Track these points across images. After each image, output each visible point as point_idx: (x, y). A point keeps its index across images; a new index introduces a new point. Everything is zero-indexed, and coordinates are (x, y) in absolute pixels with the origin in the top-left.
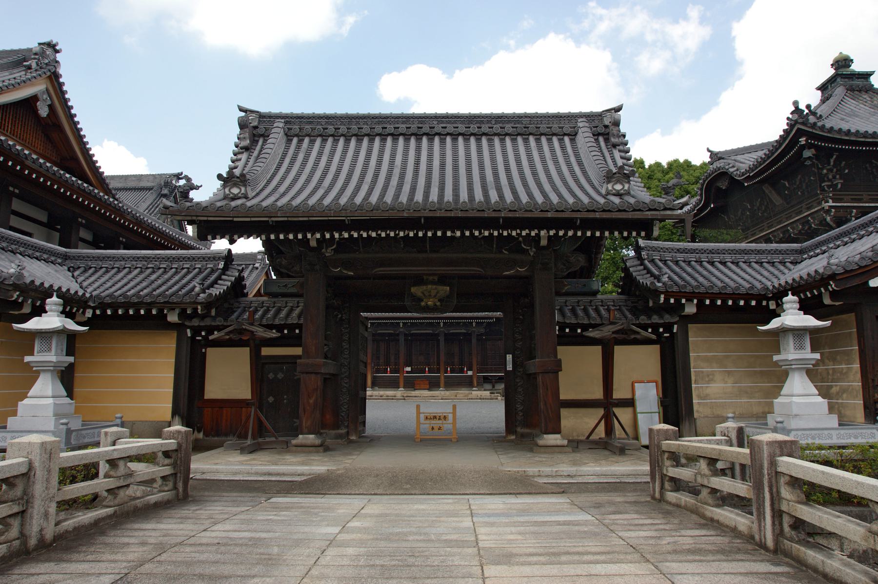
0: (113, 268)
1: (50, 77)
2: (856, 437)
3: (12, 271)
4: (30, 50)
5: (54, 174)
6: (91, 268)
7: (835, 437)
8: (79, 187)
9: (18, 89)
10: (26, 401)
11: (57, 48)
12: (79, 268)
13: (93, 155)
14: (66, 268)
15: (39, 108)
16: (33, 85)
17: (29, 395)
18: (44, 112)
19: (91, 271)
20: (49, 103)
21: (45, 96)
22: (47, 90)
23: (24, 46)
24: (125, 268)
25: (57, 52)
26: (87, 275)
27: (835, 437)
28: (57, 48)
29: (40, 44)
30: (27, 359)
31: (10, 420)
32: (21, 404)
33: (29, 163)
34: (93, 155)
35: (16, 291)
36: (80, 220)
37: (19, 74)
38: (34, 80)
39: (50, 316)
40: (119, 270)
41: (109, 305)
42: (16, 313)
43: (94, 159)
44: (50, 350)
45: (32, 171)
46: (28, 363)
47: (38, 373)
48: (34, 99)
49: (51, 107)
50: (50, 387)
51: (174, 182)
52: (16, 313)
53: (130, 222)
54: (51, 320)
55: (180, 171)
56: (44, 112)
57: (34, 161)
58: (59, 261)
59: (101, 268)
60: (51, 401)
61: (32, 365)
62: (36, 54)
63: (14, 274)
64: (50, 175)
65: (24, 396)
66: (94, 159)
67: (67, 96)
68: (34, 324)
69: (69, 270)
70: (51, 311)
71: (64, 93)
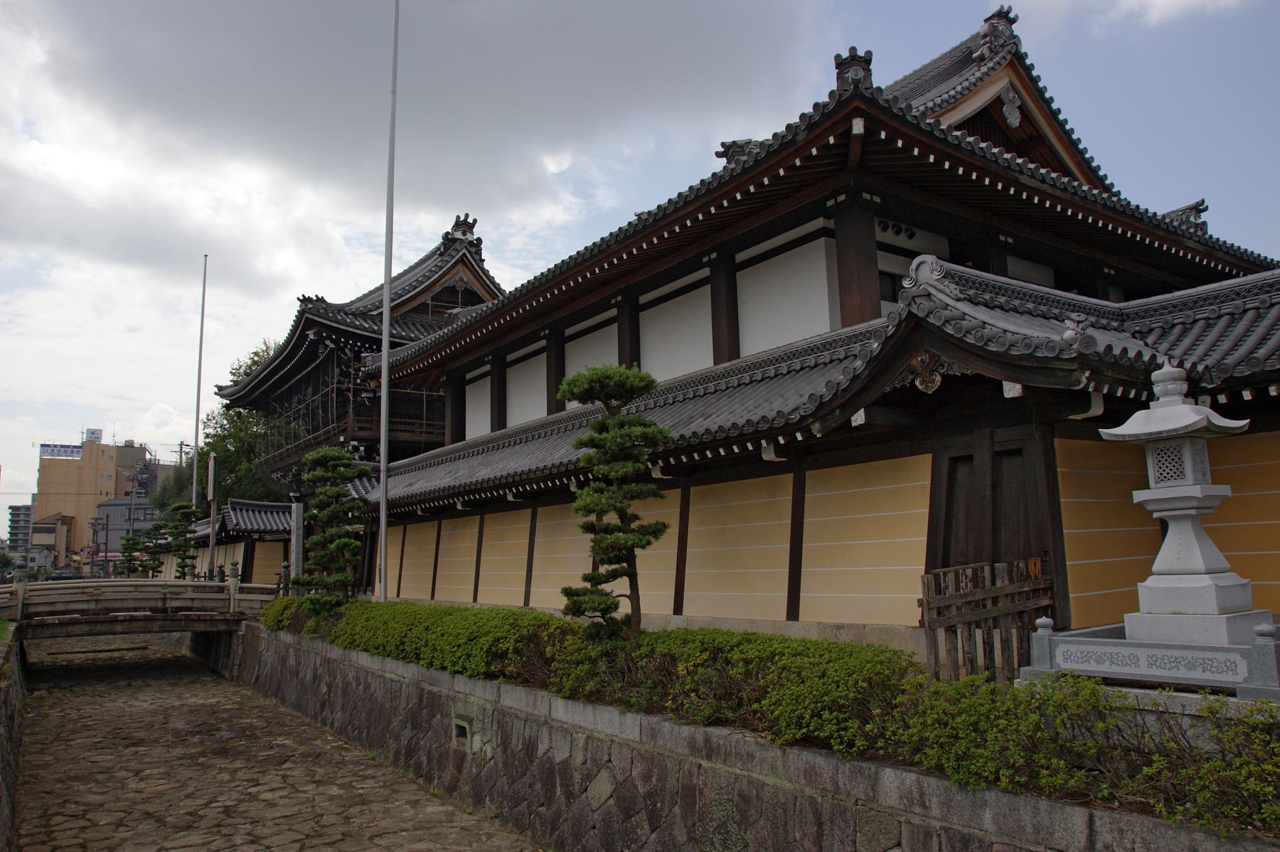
0: (1219, 317)
1: (1011, 64)
2: (1099, 661)
3: (1068, 334)
4: (977, 35)
5: (1065, 190)
6: (1174, 326)
7: (1143, 662)
8: (1105, 205)
9: (975, 94)
10: (1151, 582)
11: (1012, 15)
12: (1151, 330)
13: (1099, 167)
14: (1128, 335)
15: (1007, 114)
16: (991, 83)
17: (1155, 568)
18: (1014, 119)
19: (1177, 330)
20: (1019, 103)
21: (1011, 95)
22: (1011, 83)
23: (965, 36)
24: (1245, 311)
25: (1013, 21)
26: (1172, 338)
27: (1143, 662)
28: (1012, 15)
29: (986, 21)
30: (1139, 496)
31: (1130, 620)
32: (1141, 587)
33: (1024, 179)
34: (1099, 167)
35: (1082, 370)
36: (1106, 270)
37: (973, 74)
38: (991, 73)
39: (1165, 404)
40: (1234, 318)
41: (1245, 382)
42: (1079, 417)
43: (1101, 173)
44: (1181, 474)
45: (1032, 191)
46: (1141, 505)
47: (1163, 526)
48: (998, 102)
49: (1023, 109)
50: (1198, 552)
51: (1192, 219)
52: (1079, 417)
53: (1195, 252)
54: (1172, 413)
55: (1199, 199)
56: (1014, 119)
57: (1032, 175)
58: (1115, 324)
59: (1195, 321)
60: (1206, 580)
61: (1149, 507)
62: (985, 36)
63: (1074, 340)
64: (1058, 193)
65: (1146, 572)
66: (1101, 173)
67: (1041, 84)
68: (1137, 425)
69: (1134, 337)
70: (1166, 394)
71: (1035, 80)
